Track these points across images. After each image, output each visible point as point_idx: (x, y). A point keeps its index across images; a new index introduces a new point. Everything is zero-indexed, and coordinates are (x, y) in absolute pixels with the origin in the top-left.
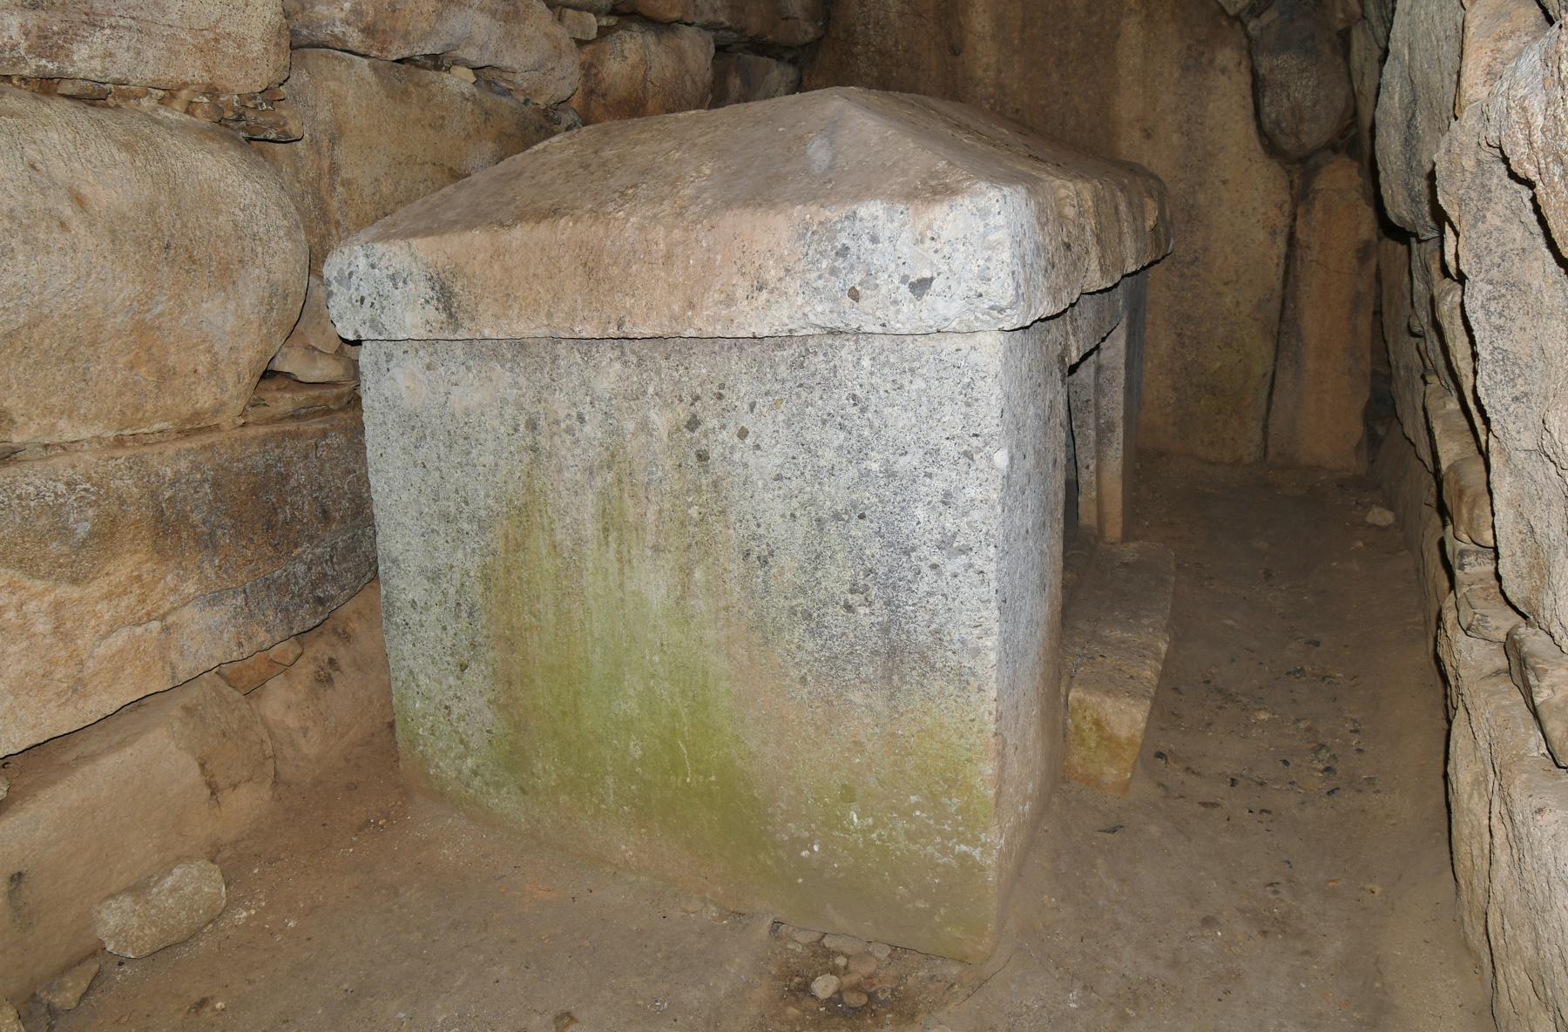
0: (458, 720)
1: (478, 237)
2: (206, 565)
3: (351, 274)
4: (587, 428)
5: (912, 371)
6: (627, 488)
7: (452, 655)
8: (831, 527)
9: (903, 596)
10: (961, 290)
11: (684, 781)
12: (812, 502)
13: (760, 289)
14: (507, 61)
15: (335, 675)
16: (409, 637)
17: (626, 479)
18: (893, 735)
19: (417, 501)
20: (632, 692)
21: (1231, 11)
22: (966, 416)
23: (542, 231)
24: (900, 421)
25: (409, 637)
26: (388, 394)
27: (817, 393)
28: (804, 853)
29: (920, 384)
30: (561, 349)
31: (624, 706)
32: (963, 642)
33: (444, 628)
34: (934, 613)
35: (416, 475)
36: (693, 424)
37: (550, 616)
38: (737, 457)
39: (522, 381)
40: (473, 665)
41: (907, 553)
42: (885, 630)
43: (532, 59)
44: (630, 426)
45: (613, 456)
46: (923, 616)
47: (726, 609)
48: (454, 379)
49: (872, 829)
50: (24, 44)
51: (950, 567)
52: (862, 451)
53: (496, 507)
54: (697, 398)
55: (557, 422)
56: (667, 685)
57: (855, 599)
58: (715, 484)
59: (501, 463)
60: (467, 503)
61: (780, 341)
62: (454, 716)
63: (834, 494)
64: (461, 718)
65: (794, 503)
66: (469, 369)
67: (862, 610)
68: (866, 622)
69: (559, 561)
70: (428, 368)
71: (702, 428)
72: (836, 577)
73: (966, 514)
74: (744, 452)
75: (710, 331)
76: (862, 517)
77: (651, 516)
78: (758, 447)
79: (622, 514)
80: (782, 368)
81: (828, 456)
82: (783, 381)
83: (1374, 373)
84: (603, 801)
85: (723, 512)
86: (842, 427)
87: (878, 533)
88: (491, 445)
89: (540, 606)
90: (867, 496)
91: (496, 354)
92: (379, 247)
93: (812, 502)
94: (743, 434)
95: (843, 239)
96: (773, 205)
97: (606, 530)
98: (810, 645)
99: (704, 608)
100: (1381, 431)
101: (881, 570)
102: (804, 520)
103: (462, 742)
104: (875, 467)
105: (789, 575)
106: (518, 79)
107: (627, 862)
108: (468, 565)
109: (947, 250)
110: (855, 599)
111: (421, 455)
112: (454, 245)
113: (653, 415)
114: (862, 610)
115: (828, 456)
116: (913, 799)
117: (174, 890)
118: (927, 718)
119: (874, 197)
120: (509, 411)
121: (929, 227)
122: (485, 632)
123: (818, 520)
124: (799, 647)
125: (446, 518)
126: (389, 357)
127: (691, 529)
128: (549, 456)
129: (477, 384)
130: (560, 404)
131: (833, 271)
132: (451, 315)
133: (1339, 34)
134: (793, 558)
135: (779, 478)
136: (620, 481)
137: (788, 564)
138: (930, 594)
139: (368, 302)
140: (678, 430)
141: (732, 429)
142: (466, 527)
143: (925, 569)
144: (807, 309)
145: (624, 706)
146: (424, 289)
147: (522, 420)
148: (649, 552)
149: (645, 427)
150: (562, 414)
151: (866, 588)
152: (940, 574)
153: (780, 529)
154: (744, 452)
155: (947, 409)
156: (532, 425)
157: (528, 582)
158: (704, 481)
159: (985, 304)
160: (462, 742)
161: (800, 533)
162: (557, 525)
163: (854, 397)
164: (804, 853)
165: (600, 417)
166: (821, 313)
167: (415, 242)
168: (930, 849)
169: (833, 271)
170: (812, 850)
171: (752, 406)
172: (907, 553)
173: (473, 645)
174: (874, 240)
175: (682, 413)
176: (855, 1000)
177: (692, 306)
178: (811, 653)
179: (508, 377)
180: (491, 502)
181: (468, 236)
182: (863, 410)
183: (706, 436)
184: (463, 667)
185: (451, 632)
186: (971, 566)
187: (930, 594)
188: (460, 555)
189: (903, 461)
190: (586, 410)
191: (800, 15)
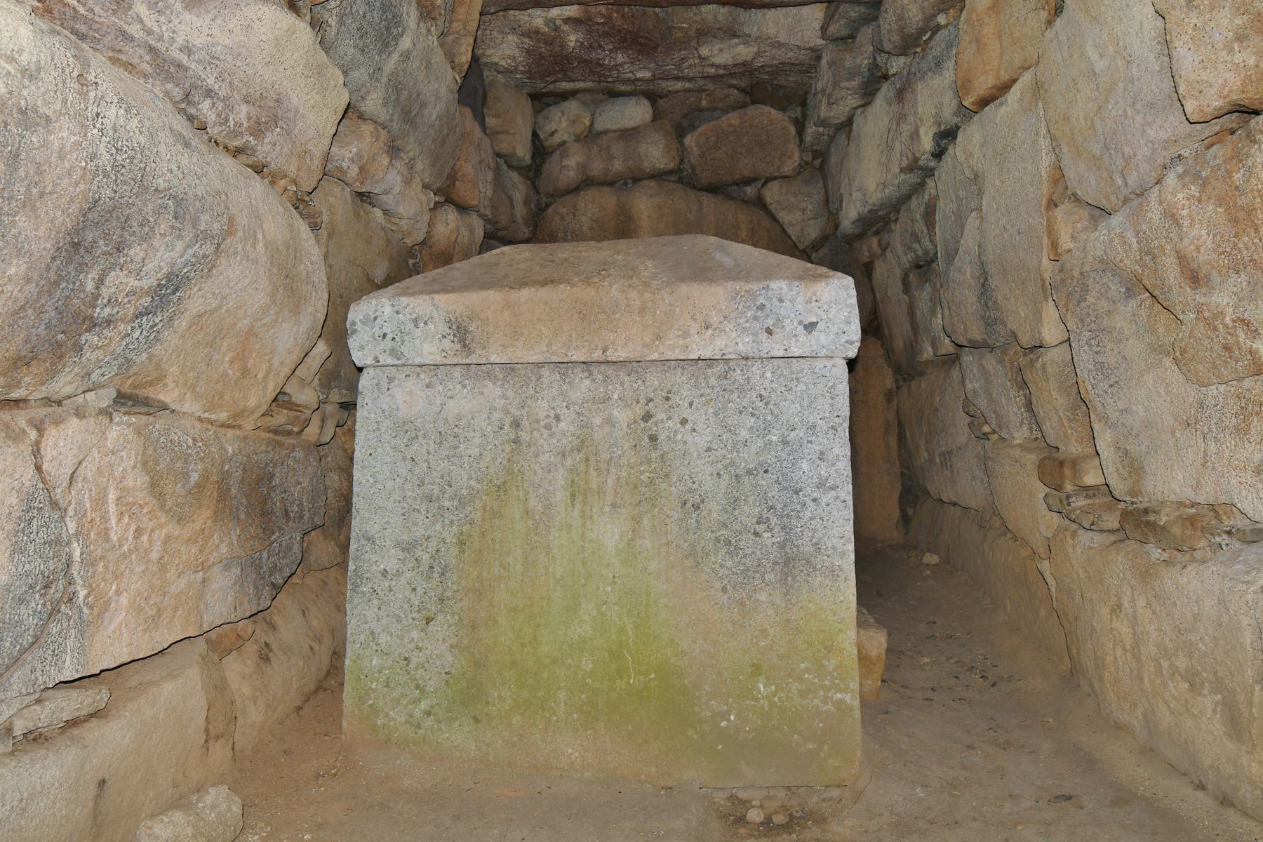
0: (417, 668)
1: (492, 295)
2: (232, 532)
3: (376, 318)
4: (563, 425)
5: (797, 379)
6: (592, 463)
7: (419, 611)
8: (746, 480)
9: (794, 522)
10: (835, 329)
11: (628, 683)
12: (732, 464)
13: (707, 328)
14: (401, 210)
15: (271, 655)
16: (375, 602)
17: (592, 458)
18: (788, 621)
19: (402, 488)
20: (586, 618)
21: (801, 247)
22: (832, 405)
23: (545, 293)
24: (791, 409)
25: (375, 602)
26: (385, 407)
27: (736, 395)
28: (723, 724)
29: (802, 387)
30: (545, 372)
31: (579, 630)
32: (834, 548)
33: (414, 589)
34: (815, 531)
35: (403, 469)
36: (647, 417)
37: (519, 567)
38: (679, 437)
39: (510, 393)
40: (440, 617)
41: (796, 493)
42: (782, 546)
43: (412, 211)
44: (597, 421)
45: (582, 442)
46: (807, 534)
47: (667, 544)
48: (450, 394)
49: (774, 694)
50: (245, 125)
51: (825, 500)
52: (767, 429)
53: (477, 486)
54: (651, 400)
55: (538, 421)
56: (616, 607)
57: (760, 528)
58: (662, 457)
59: (485, 453)
60: (450, 486)
61: (711, 361)
62: (412, 666)
63: (748, 458)
64: (420, 666)
65: (720, 466)
66: (464, 386)
67: (766, 535)
68: (769, 542)
69: (530, 523)
70: (428, 386)
71: (654, 419)
72: (749, 512)
73: (834, 465)
74: (683, 434)
75: (669, 355)
76: (766, 471)
77: (611, 482)
78: (694, 430)
79: (587, 482)
80: (713, 379)
81: (744, 433)
82: (713, 387)
83: (902, 474)
84: (554, 714)
85: (667, 476)
86: (753, 415)
87: (777, 482)
88: (477, 440)
89: (510, 560)
90: (770, 458)
91: (490, 376)
92: (404, 300)
93: (732, 464)
94: (684, 422)
95: (761, 300)
96: (713, 281)
97: (573, 495)
98: (729, 564)
99: (650, 546)
100: (910, 512)
101: (779, 506)
102: (726, 477)
103: (418, 687)
104: (775, 439)
105: (715, 515)
106: (403, 222)
107: (572, 763)
108: (445, 534)
109: (825, 307)
110: (760, 528)
111: (410, 452)
112: (475, 299)
113: (615, 412)
114: (766, 535)
115: (744, 433)
116: (803, 666)
117: (213, 807)
118: (812, 605)
119: (779, 278)
120: (496, 416)
121: (814, 294)
122: (455, 588)
123: (736, 476)
124: (721, 566)
125: (430, 499)
126: (391, 380)
127: (643, 489)
128: (529, 445)
129: (469, 396)
130: (542, 408)
131: (755, 318)
132: (465, 346)
133: (864, 265)
134: (718, 503)
135: (709, 449)
136: (587, 460)
137: (714, 510)
138: (812, 518)
139: (389, 337)
140: (635, 422)
141: (676, 419)
142: (447, 504)
143: (809, 502)
144: (738, 340)
145: (579, 630)
146: (443, 328)
147: (508, 421)
148: (607, 509)
149: (610, 421)
150: (542, 415)
151: (768, 519)
152: (818, 505)
153: (709, 484)
154: (683, 434)
155: (820, 401)
156: (516, 424)
157: (501, 542)
158: (654, 455)
159: (845, 338)
160: (418, 687)
161: (723, 485)
162: (531, 495)
163: (761, 396)
164: (723, 724)
165: (574, 416)
166: (745, 345)
167: (437, 297)
168: (816, 701)
169: (755, 318)
170: (729, 720)
171: (691, 404)
172: (796, 493)
173: (442, 600)
174: (781, 301)
175: (639, 410)
176: (779, 819)
177: (658, 338)
178: (730, 569)
179: (498, 391)
180: (472, 483)
181: (484, 294)
182: (767, 404)
183: (656, 424)
184: (428, 620)
185: (420, 591)
186: (838, 497)
187: (812, 518)
188: (438, 527)
189: (793, 434)
190: (562, 411)
191: (521, 221)
